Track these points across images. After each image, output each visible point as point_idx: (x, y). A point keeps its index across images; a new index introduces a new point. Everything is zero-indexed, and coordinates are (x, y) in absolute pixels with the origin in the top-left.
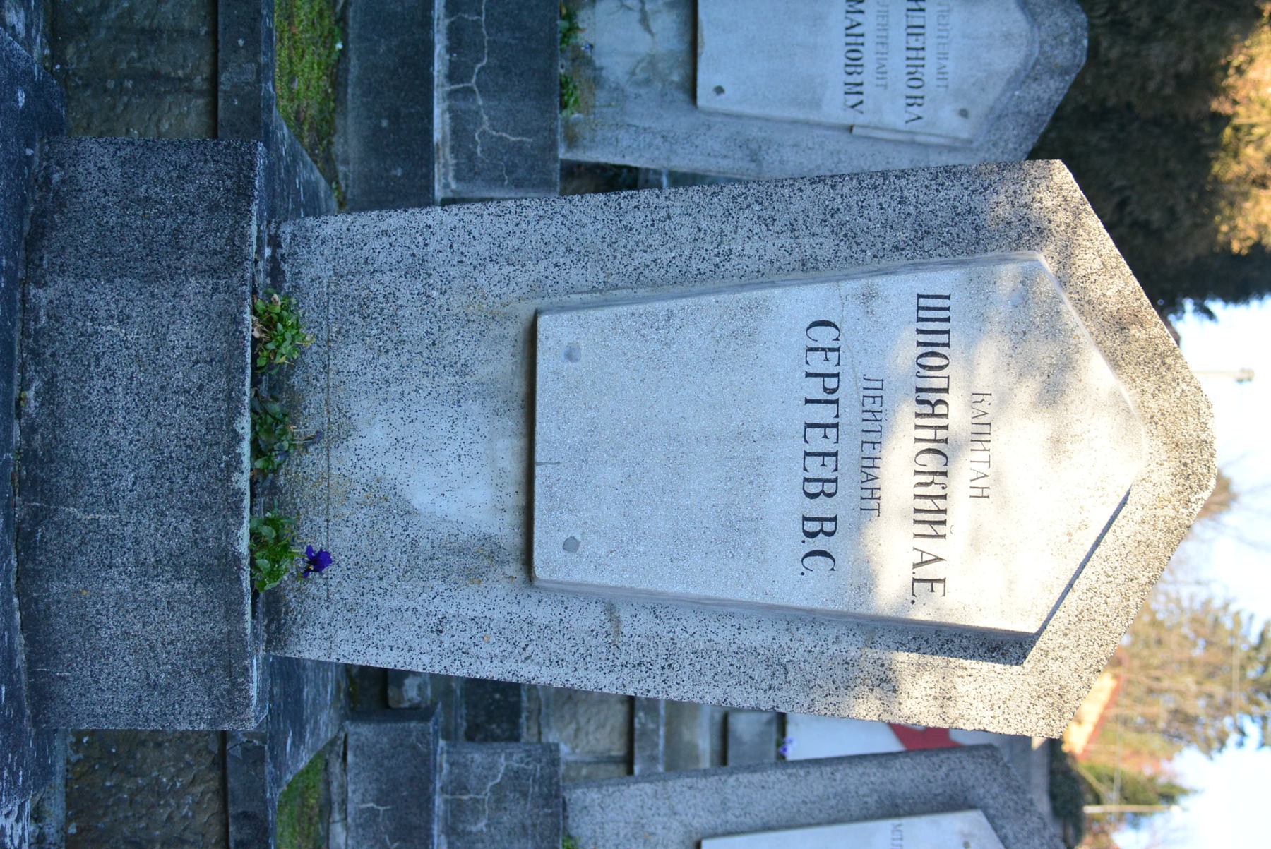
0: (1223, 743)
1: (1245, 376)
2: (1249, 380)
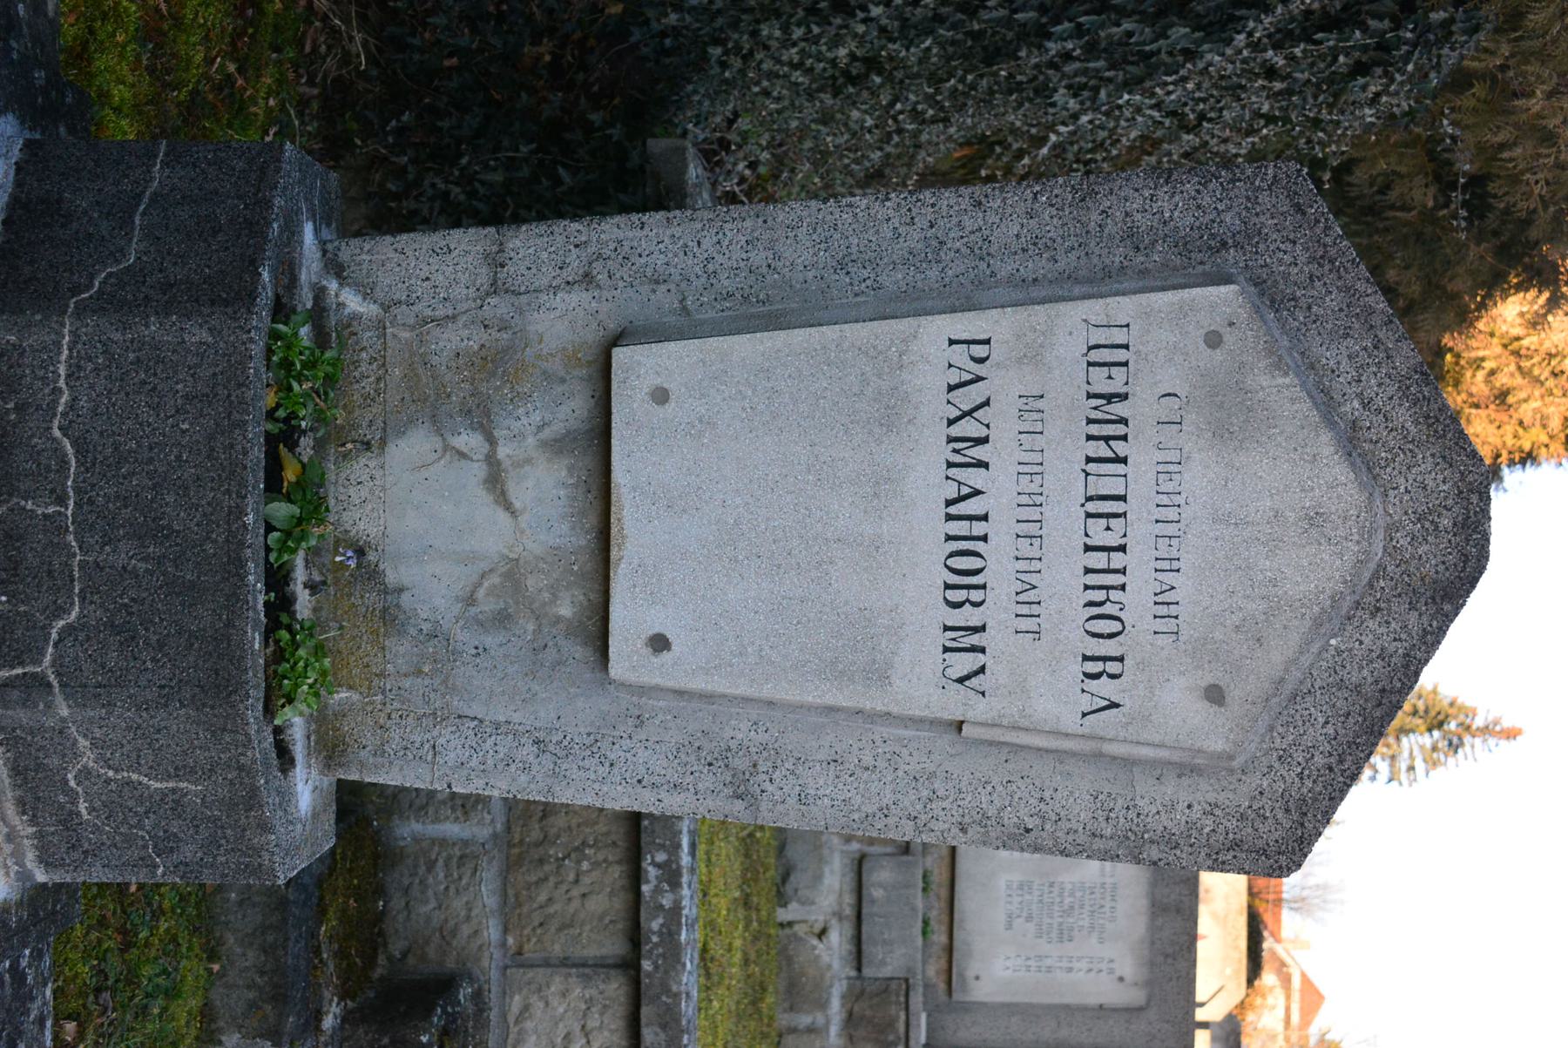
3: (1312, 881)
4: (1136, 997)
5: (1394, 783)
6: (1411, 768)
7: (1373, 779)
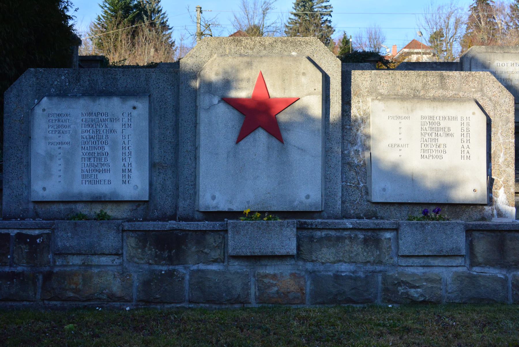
0: (330, 27)
1: (199, 9)
2: (201, 8)
3: (368, 43)
5: (332, 14)
6: (326, 7)
7: (330, 22)
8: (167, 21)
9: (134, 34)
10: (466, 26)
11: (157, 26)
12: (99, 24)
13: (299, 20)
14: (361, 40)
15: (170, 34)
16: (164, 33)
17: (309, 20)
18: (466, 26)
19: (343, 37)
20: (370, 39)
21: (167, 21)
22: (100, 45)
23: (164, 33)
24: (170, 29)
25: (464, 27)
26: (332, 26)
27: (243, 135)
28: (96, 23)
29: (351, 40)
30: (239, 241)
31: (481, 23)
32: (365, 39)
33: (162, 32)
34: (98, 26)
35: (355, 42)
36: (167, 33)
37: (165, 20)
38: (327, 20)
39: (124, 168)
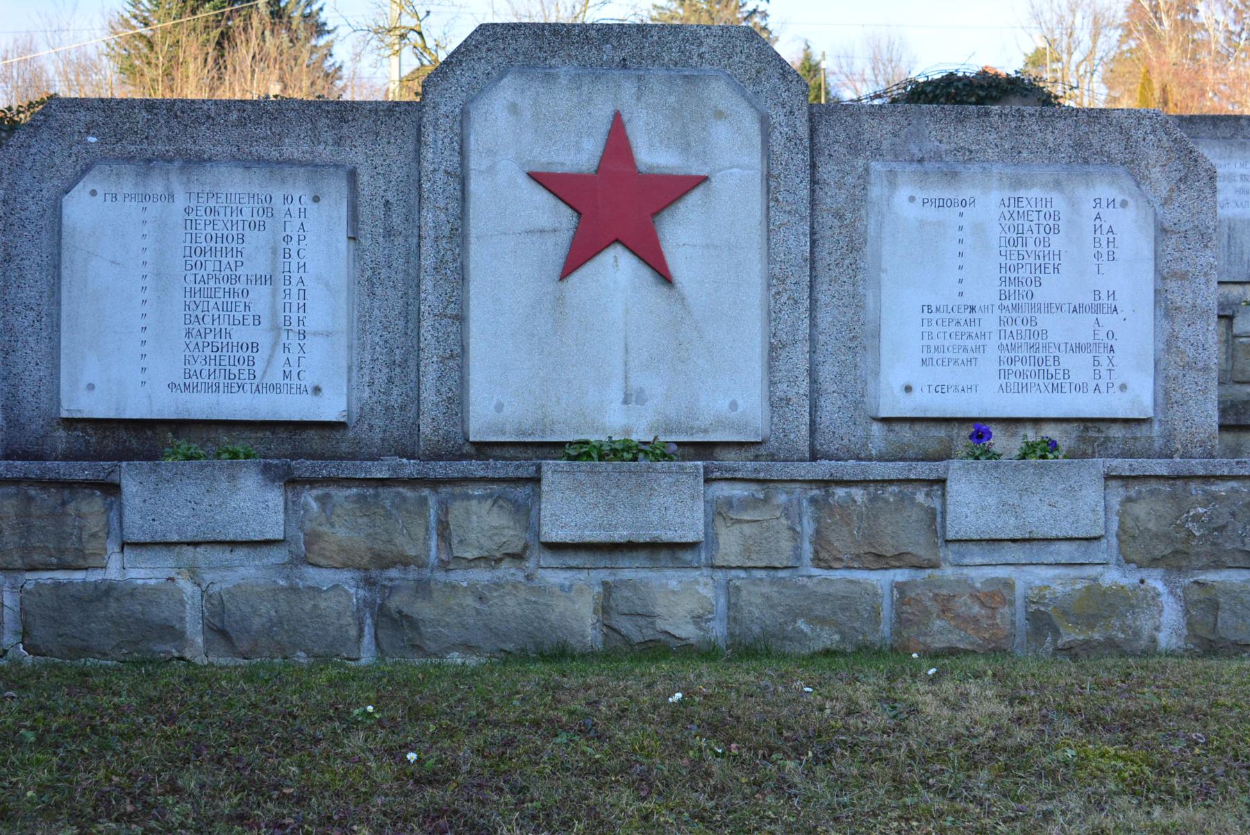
3: (869, 74)
4: (336, 192)
7: (765, 15)
8: (321, 9)
9: (224, 40)
10: (1119, 31)
11: (295, 23)
12: (135, 17)
13: (681, 11)
14: (850, 65)
15: (329, 46)
16: (313, 42)
17: (708, 11)
18: (1119, 31)
19: (802, 55)
20: (875, 61)
21: (321, 9)
22: (129, 71)
23: (313, 42)
24: (329, 32)
25: (1116, 34)
26: (770, 27)
27: (579, 256)
28: (127, 15)
29: (823, 65)
30: (568, 508)
31: (1161, 23)
32: (862, 64)
33: (307, 40)
34: (134, 22)
35: (836, 69)
36: (322, 42)
37: (315, 7)
38: (755, 11)
39: (287, 369)
